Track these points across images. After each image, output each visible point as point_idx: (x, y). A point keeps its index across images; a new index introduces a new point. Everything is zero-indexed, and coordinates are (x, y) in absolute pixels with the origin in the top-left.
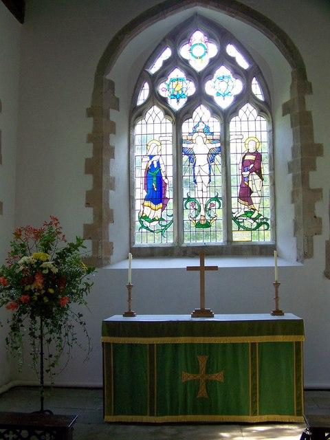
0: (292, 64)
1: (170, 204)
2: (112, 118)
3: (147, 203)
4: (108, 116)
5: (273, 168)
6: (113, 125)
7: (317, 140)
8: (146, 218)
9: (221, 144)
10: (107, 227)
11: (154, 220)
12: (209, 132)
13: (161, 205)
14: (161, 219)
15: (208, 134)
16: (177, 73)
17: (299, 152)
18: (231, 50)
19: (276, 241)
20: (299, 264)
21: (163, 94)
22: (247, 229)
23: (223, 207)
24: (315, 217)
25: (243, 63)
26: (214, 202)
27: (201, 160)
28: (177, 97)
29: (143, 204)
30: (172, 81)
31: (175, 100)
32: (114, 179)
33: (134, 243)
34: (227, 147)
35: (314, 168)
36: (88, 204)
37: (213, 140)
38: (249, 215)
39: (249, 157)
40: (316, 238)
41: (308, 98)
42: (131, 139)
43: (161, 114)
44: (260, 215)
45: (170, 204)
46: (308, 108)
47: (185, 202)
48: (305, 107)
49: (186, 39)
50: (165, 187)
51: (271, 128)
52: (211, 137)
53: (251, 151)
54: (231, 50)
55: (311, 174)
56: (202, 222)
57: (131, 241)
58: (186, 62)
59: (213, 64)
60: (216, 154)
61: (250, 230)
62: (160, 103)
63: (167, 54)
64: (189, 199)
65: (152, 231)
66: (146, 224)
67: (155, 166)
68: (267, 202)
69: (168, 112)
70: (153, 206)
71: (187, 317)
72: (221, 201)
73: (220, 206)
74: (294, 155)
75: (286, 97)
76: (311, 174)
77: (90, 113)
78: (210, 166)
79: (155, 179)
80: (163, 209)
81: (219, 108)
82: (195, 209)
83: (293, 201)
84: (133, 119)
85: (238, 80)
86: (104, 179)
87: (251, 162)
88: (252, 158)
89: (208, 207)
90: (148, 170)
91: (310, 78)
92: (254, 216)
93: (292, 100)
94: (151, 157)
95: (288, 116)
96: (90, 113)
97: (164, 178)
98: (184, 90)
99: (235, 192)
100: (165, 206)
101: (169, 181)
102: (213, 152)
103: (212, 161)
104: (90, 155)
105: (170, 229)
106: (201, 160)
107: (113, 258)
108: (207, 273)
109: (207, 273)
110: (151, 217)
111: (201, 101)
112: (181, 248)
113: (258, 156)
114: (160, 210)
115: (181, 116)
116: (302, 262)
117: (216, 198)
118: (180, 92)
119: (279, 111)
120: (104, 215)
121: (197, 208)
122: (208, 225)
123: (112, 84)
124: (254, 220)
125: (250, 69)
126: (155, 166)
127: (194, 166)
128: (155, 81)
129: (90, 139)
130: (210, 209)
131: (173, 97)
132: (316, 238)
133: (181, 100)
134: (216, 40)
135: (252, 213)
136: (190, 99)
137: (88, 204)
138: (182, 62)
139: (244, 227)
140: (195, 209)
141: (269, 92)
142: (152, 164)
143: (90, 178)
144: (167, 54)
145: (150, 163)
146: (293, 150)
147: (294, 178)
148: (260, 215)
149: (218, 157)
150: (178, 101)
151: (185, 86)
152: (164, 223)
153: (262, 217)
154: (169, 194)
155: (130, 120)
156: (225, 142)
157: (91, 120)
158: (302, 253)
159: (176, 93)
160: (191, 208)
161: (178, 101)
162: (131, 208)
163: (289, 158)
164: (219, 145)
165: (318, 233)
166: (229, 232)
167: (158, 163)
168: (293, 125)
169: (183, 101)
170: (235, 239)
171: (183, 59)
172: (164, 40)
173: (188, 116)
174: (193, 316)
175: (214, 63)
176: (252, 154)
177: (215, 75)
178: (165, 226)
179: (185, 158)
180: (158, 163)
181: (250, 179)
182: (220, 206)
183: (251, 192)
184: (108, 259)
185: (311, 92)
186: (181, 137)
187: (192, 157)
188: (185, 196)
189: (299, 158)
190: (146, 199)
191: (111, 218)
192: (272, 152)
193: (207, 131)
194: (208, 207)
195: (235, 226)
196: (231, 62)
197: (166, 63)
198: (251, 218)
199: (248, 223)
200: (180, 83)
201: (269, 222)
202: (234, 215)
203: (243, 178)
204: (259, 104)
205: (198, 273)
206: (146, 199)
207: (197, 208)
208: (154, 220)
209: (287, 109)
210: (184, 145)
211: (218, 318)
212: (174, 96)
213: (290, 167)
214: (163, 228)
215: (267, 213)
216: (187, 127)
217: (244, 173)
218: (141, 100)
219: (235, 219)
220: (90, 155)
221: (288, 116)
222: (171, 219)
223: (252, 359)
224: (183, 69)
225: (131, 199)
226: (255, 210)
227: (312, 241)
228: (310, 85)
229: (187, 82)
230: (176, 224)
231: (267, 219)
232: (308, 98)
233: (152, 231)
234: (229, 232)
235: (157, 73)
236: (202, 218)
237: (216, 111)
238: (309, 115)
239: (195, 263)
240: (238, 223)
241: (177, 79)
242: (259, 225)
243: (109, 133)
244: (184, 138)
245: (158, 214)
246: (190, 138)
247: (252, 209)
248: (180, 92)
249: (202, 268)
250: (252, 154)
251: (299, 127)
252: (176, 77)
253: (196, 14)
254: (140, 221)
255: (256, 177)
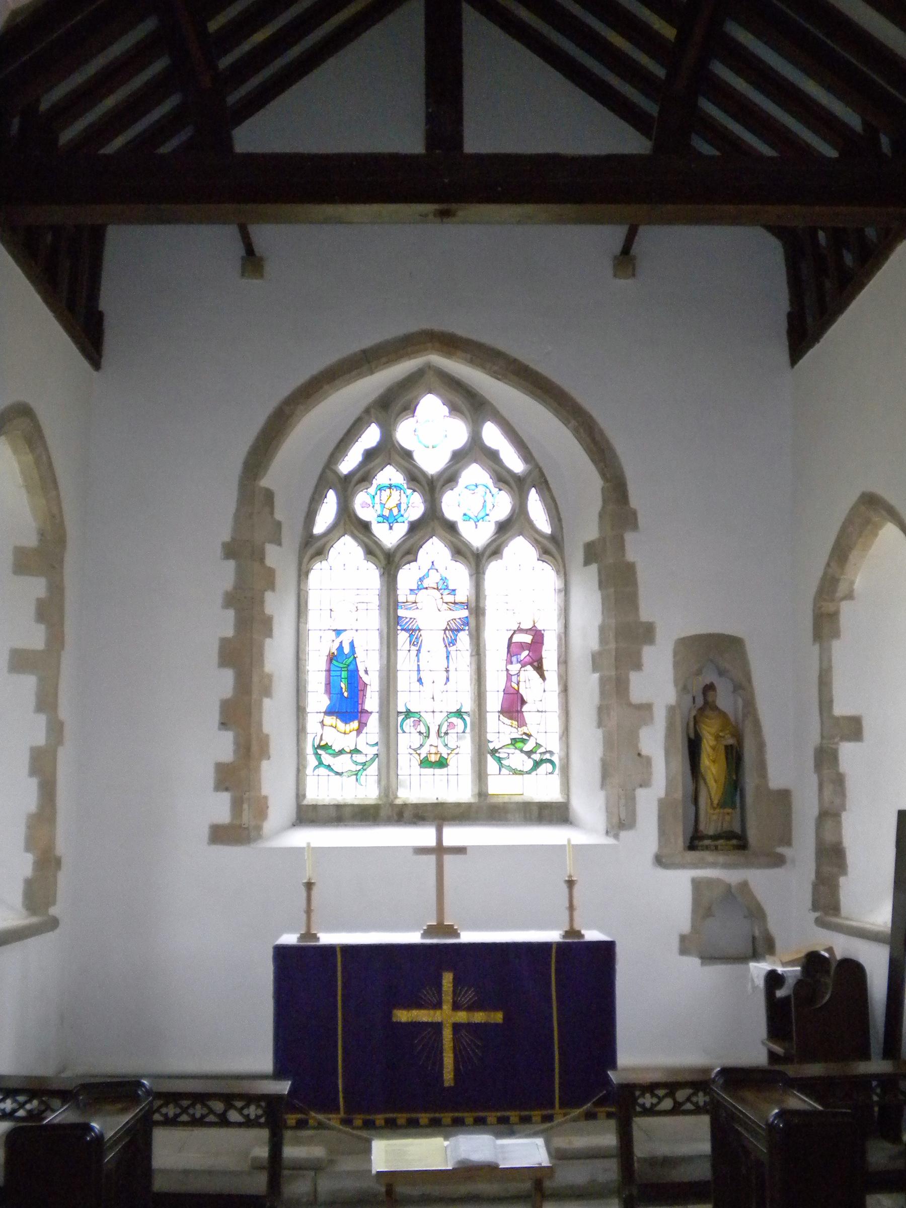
0: (603, 475)
1: (373, 723)
2: (270, 561)
3: (330, 720)
4: (262, 559)
5: (564, 661)
6: (271, 573)
7: (645, 616)
8: (326, 747)
9: (470, 613)
10: (258, 770)
11: (341, 752)
12: (447, 588)
13: (355, 725)
14: (356, 751)
15: (447, 592)
16: (390, 475)
17: (612, 635)
18: (492, 435)
19: (568, 796)
20: (610, 841)
21: (364, 513)
22: (516, 772)
23: (472, 730)
24: (639, 755)
25: (515, 463)
26: (454, 720)
27: (433, 640)
28: (389, 520)
29: (322, 722)
30: (380, 489)
31: (386, 525)
32: (270, 677)
33: (304, 796)
34: (481, 618)
35: (638, 666)
36: (224, 725)
37: (455, 603)
38: (519, 745)
39: (520, 638)
40: (641, 793)
41: (629, 537)
42: (302, 598)
43: (359, 552)
44: (538, 745)
45: (373, 723)
46: (630, 556)
47: (400, 718)
48: (624, 556)
49: (409, 409)
50: (364, 690)
51: (562, 586)
52: (450, 598)
53: (523, 627)
54: (492, 435)
55: (634, 677)
56: (433, 758)
57: (300, 795)
58: (408, 455)
59: (457, 462)
60: (458, 630)
61: (521, 773)
62: (356, 532)
63: (371, 436)
64: (408, 713)
65: (337, 773)
66: (326, 758)
67: (347, 650)
68: (554, 723)
69: (372, 549)
70: (341, 725)
71: (414, 937)
72: (468, 719)
73: (465, 726)
74: (603, 640)
75: (592, 533)
76: (634, 677)
77: (231, 551)
78: (448, 653)
79: (344, 674)
80: (359, 731)
81: (467, 545)
82: (420, 733)
83: (600, 724)
84: (305, 560)
85: (502, 492)
86: (255, 679)
87: (522, 646)
88: (527, 639)
89: (444, 729)
90: (332, 658)
91: (635, 501)
92: (528, 747)
93: (602, 539)
94: (338, 632)
95: (594, 567)
96: (231, 551)
97: (362, 673)
98: (403, 507)
99: (494, 701)
100: (362, 725)
101: (372, 681)
102: (453, 626)
103: (453, 642)
104: (229, 632)
105: (373, 769)
106: (433, 640)
107: (268, 826)
108: (448, 859)
109: (448, 859)
110: (337, 748)
111: (433, 529)
112: (392, 805)
113: (538, 637)
114: (355, 733)
115: (397, 559)
116: (616, 836)
117: (459, 713)
118: (395, 511)
119: (576, 555)
120: (255, 748)
121: (423, 730)
122: (442, 763)
123: (269, 496)
124: (529, 754)
125: (529, 473)
126: (347, 650)
127: (419, 651)
128: (350, 489)
129: (230, 600)
130: (446, 734)
131: (381, 519)
132: (641, 793)
133: (395, 526)
134: (511, 487)
135: (524, 741)
136: (414, 527)
137: (224, 725)
138: (399, 454)
139: (509, 767)
140: (420, 733)
141: (560, 520)
142: (341, 648)
143: (227, 677)
144: (371, 436)
145: (336, 645)
146: (602, 629)
147: (603, 682)
148: (538, 745)
149: (464, 638)
150: (391, 528)
151: (404, 500)
152: (360, 758)
153: (542, 750)
154: (372, 702)
155: (300, 564)
156: (477, 609)
157: (231, 564)
158: (615, 820)
159: (386, 513)
160: (413, 730)
161: (391, 528)
162: (301, 730)
163: (594, 644)
164: (465, 613)
165: (645, 783)
166: (481, 775)
167: (352, 645)
168: (602, 585)
169: (401, 529)
170: (492, 790)
171: (402, 448)
172: (367, 411)
173: (410, 557)
174: (426, 934)
175: (460, 458)
176: (526, 631)
177: (461, 480)
178: (364, 764)
179: (402, 637)
180: (352, 645)
181: (522, 678)
182: (465, 726)
183: (523, 702)
184: (259, 828)
185: (635, 526)
186: (396, 596)
187: (414, 632)
188: (401, 708)
189: (612, 646)
190: (329, 712)
191: (264, 752)
192: (563, 630)
193: (443, 587)
194: (444, 729)
195: (492, 765)
196: (491, 458)
197: (369, 455)
198: (522, 751)
199: (518, 760)
200: (396, 494)
201: (556, 759)
202: (491, 746)
203: (509, 676)
204: (540, 539)
205: (432, 858)
206: (329, 712)
207: (423, 730)
208: (341, 752)
209: (592, 553)
210: (401, 613)
211: (467, 937)
212: (384, 518)
213: (596, 662)
214: (359, 767)
215: (552, 742)
216: (407, 576)
217: (509, 667)
218: (322, 523)
219: (494, 752)
220: (229, 632)
221: (594, 567)
222: (375, 750)
223: (746, 1129)
224: (400, 468)
225: (300, 711)
226: (529, 736)
227: (633, 799)
228: (634, 513)
229: (409, 492)
230: (384, 761)
231: (551, 753)
232: (629, 537)
233: (337, 773)
234: (481, 775)
235: (352, 474)
236: (433, 750)
237: (460, 550)
238: (630, 569)
239: (425, 836)
240: (499, 760)
241: (390, 487)
242: (537, 764)
243: (265, 590)
244: (401, 598)
245: (347, 743)
246: (411, 598)
247: (525, 734)
248: (395, 511)
249: (440, 850)
250: (526, 631)
251: (612, 590)
252: (387, 483)
253: (429, 366)
254: (316, 754)
255: (534, 675)
